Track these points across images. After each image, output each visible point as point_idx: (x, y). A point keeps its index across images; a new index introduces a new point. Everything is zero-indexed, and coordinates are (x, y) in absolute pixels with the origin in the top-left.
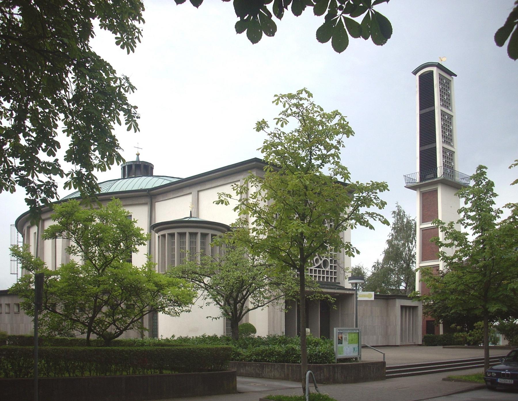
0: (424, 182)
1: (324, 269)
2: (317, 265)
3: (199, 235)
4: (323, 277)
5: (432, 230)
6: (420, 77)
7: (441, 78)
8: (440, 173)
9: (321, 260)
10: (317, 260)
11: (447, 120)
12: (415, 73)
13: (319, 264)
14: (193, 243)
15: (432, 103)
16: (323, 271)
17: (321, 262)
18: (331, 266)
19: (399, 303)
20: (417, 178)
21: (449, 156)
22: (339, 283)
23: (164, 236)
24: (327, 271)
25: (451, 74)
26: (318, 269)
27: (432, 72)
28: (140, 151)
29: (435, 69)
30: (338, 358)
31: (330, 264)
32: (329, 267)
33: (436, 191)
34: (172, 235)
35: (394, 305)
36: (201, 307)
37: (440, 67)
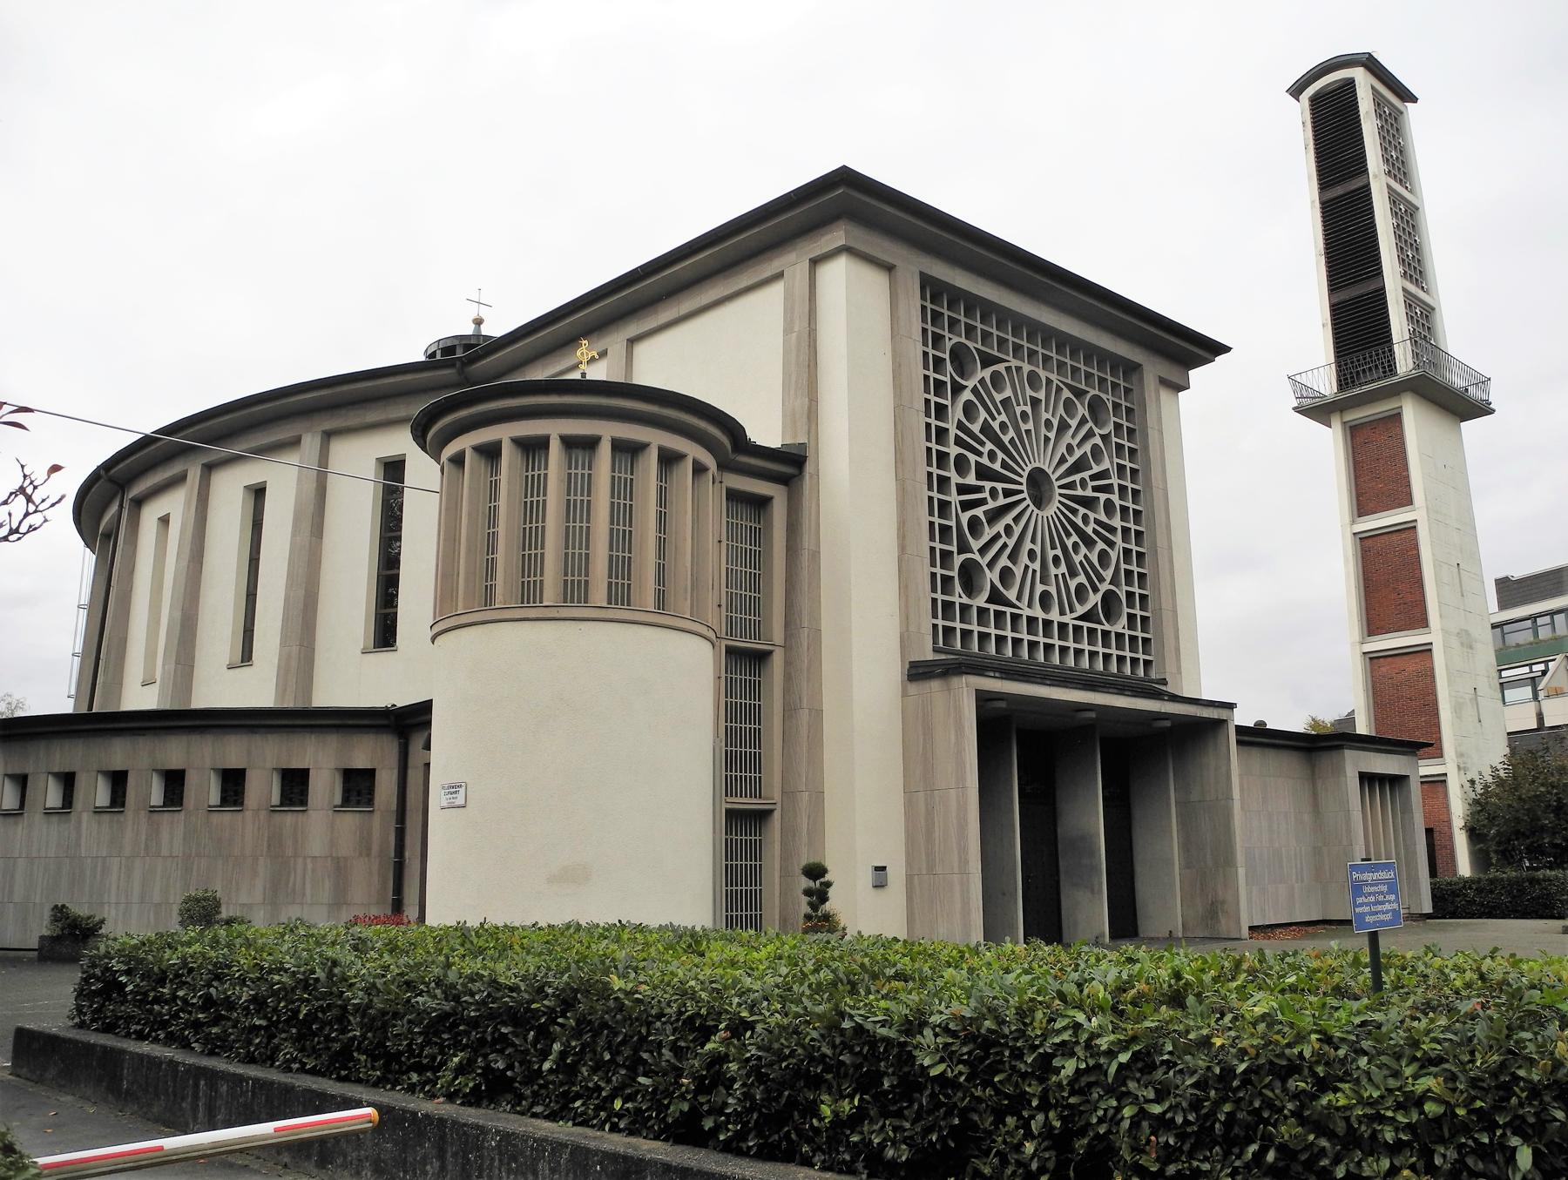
0: (1357, 391)
1: (1107, 627)
2: (1081, 610)
3: (605, 450)
4: (1107, 657)
5: (1394, 537)
6: (1314, 100)
7: (1379, 101)
8: (1404, 361)
9: (1096, 590)
10: (1080, 589)
11: (1407, 217)
12: (1296, 91)
13: (1088, 606)
14: (578, 486)
15: (1359, 164)
16: (1106, 634)
17: (1094, 599)
18: (1131, 617)
19: (1356, 762)
20: (1325, 384)
21: (1423, 316)
22: (1164, 682)
23: (458, 460)
24: (1119, 636)
26: (1086, 625)
27: (1350, 83)
28: (484, 313)
29: (1360, 75)
30: (961, 917)
31: (1126, 610)
32: (1124, 620)
33: (1396, 418)
34: (490, 453)
35: (1339, 770)
36: (55, 468)
37: (1370, 64)
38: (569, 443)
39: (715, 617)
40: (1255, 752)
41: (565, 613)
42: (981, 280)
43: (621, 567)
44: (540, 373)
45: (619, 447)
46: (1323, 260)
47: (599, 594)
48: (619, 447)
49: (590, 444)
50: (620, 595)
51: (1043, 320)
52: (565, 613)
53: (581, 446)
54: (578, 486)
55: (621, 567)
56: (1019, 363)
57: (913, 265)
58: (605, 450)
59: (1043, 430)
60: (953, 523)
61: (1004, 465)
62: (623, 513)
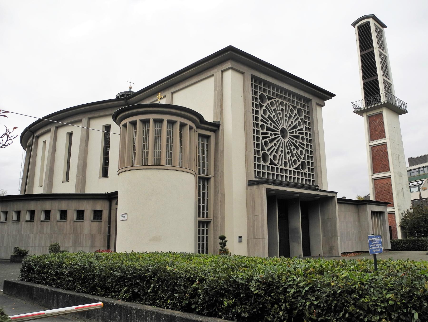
1: (302, 171)
2: (295, 166)
3: (165, 123)
4: (302, 179)
6: (359, 27)
7: (376, 28)
8: (383, 99)
9: (299, 161)
10: (295, 161)
11: (384, 59)
12: (354, 25)
13: (297, 165)
14: (158, 133)
15: (371, 45)
16: (302, 173)
17: (299, 163)
18: (309, 168)
19: (370, 208)
20: (362, 105)
21: (388, 86)
22: (318, 186)
23: (125, 126)
24: (306, 174)
25: (384, 26)
26: (296, 170)
27: (369, 23)
28: (132, 85)
29: (371, 21)
31: (307, 166)
32: (307, 169)
33: (381, 114)
34: (134, 124)
35: (366, 210)
38: (155, 121)
39: (195, 168)
40: (343, 205)
41: (154, 167)
42: (268, 77)
43: (169, 155)
44: (147, 102)
45: (169, 122)
46: (361, 71)
47: (164, 162)
48: (169, 122)
49: (161, 121)
50: (169, 162)
51: (285, 87)
52: (154, 167)
53: (158, 122)
54: (158, 133)
55: (169, 155)
56: (278, 99)
57: (249, 72)
58: (165, 123)
59: (285, 117)
60: (260, 143)
61: (274, 127)
62: (170, 140)
